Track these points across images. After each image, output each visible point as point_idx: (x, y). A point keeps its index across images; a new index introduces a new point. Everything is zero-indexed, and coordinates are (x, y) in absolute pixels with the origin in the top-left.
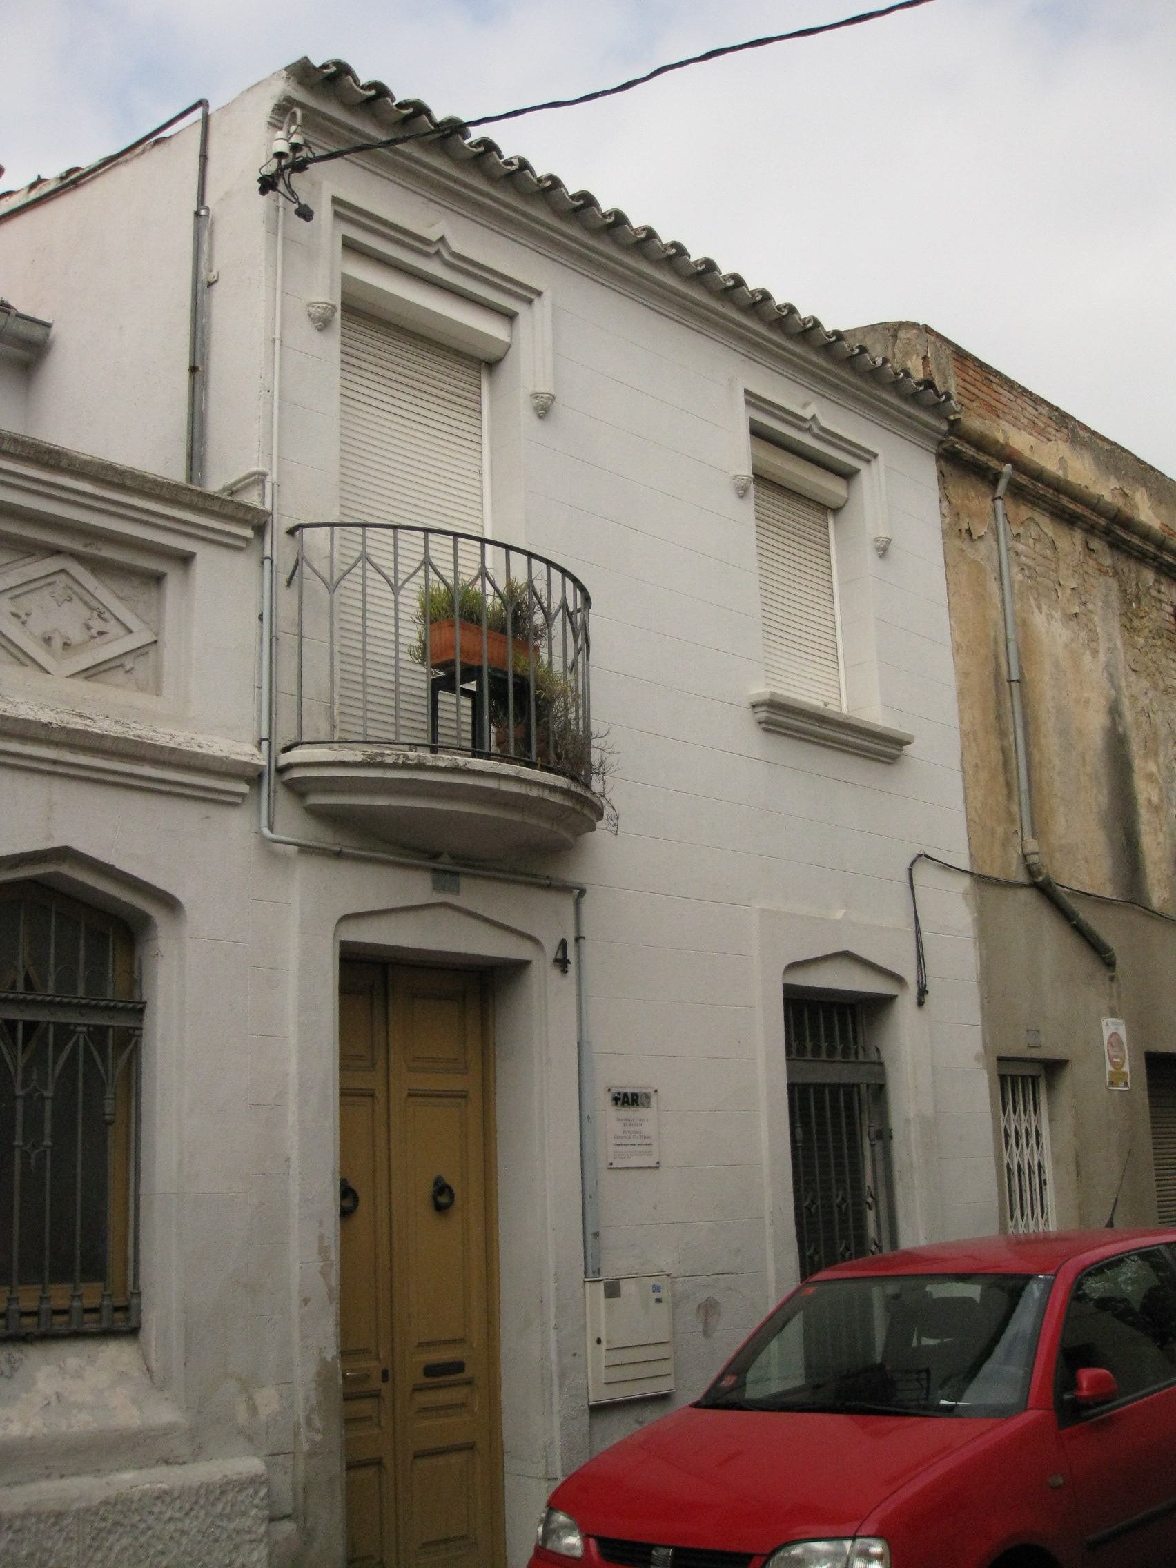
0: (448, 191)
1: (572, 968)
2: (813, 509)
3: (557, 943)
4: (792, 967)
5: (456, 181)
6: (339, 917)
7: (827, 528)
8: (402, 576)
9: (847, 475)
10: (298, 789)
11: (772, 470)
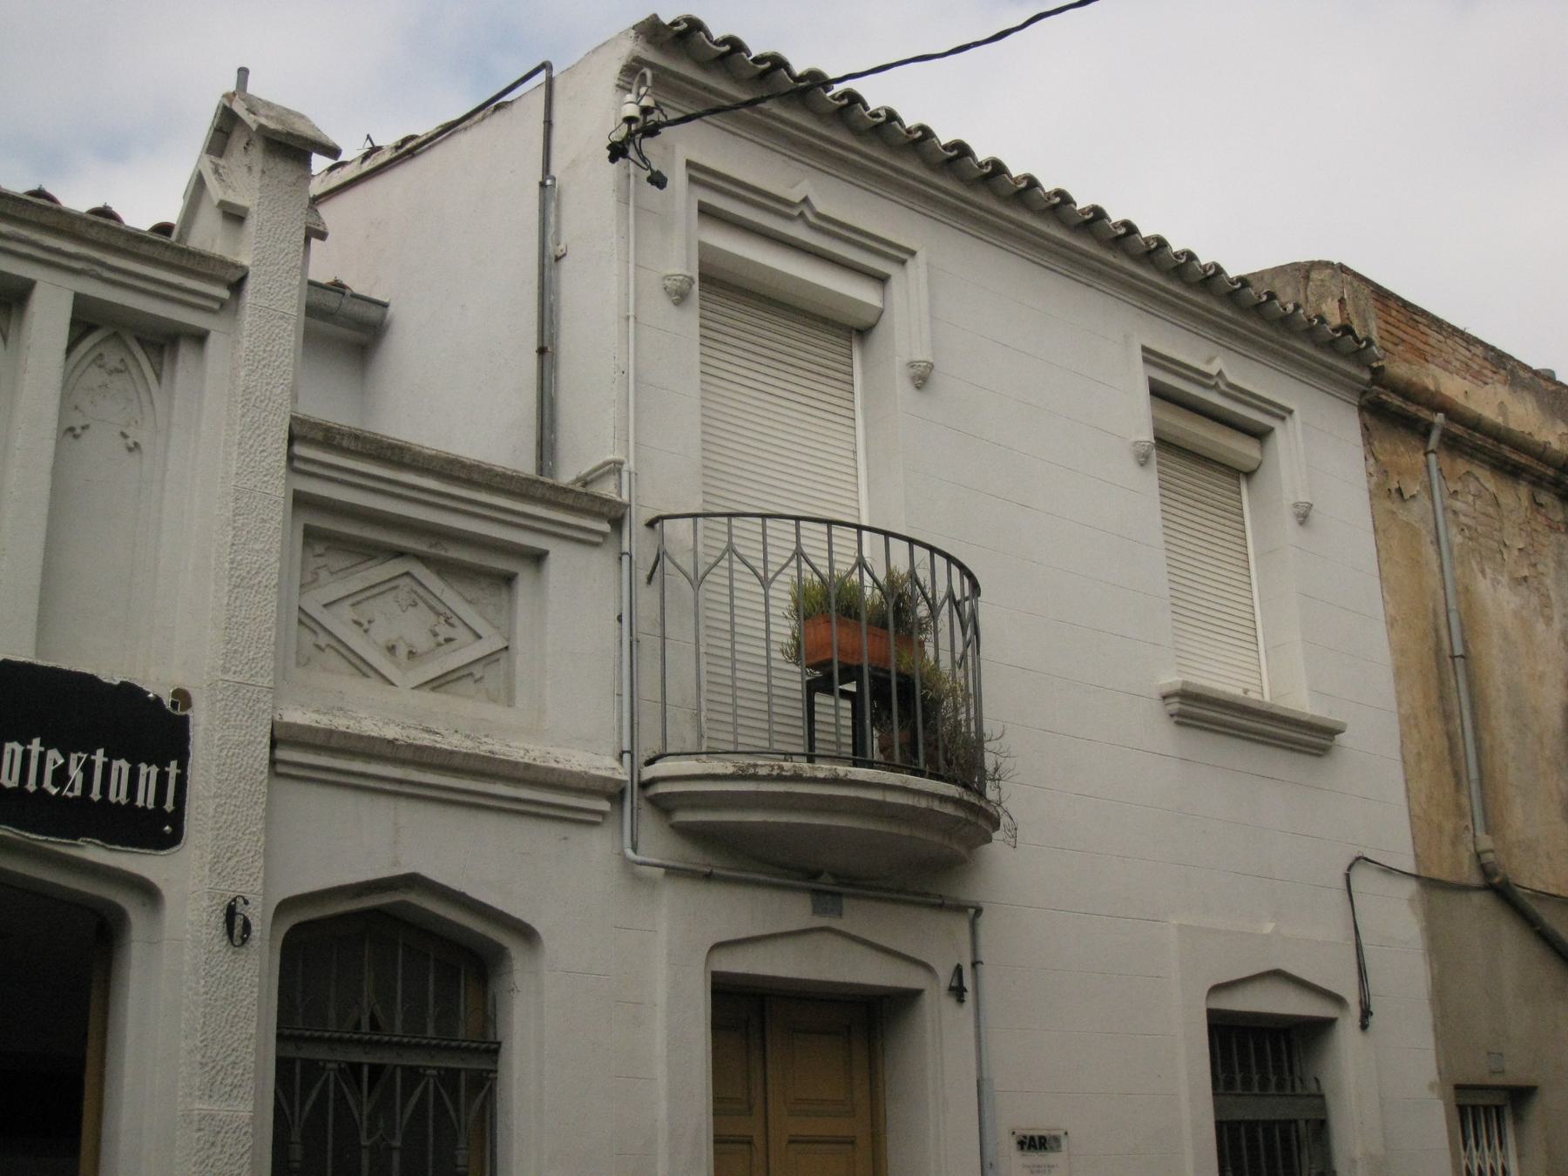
3: (952, 968)
7: (1239, 493)
9: (1260, 435)
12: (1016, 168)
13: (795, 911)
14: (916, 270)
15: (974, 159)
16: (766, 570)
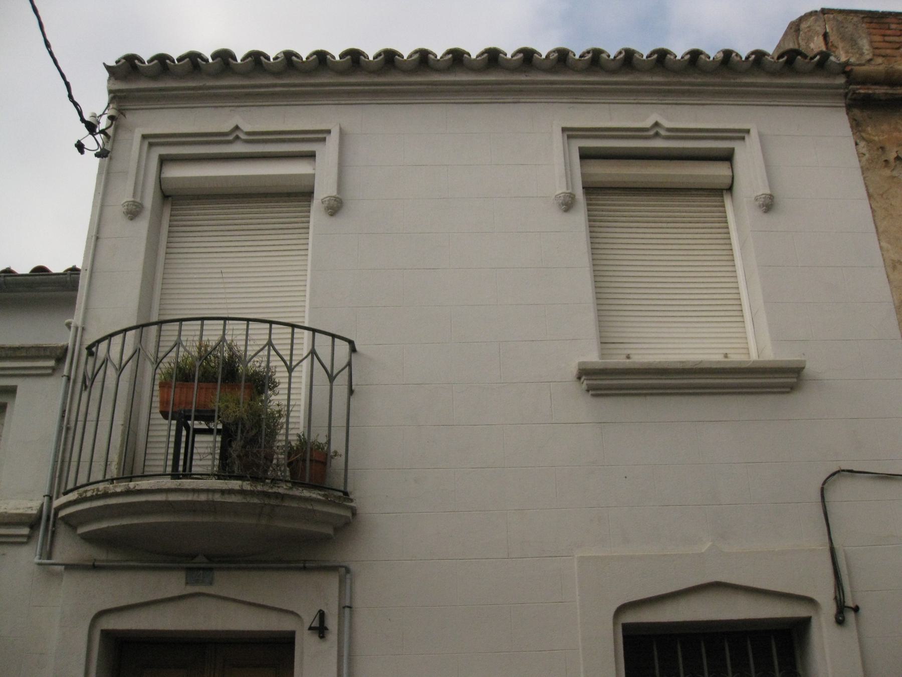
0: (248, 96)
1: (332, 636)
2: (620, 194)
3: (315, 612)
4: (622, 609)
5: (243, 87)
6: (94, 612)
7: (724, 206)
8: (265, 352)
9: (727, 157)
10: (72, 522)
11: (610, 179)
12: (273, 51)
13: (173, 583)
14: (753, 140)
15: (769, 55)
16: (291, 362)
